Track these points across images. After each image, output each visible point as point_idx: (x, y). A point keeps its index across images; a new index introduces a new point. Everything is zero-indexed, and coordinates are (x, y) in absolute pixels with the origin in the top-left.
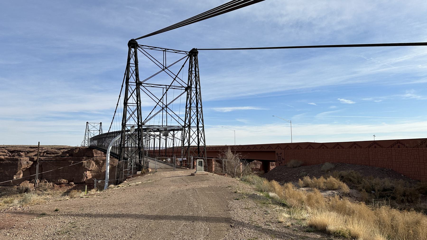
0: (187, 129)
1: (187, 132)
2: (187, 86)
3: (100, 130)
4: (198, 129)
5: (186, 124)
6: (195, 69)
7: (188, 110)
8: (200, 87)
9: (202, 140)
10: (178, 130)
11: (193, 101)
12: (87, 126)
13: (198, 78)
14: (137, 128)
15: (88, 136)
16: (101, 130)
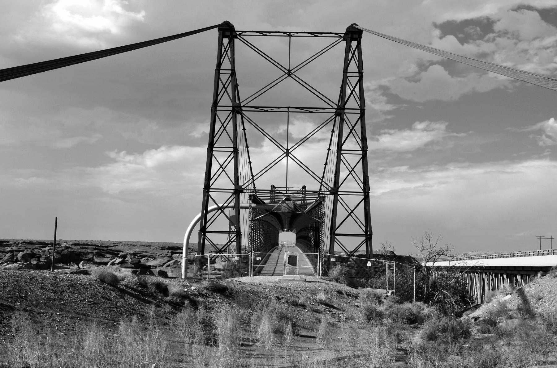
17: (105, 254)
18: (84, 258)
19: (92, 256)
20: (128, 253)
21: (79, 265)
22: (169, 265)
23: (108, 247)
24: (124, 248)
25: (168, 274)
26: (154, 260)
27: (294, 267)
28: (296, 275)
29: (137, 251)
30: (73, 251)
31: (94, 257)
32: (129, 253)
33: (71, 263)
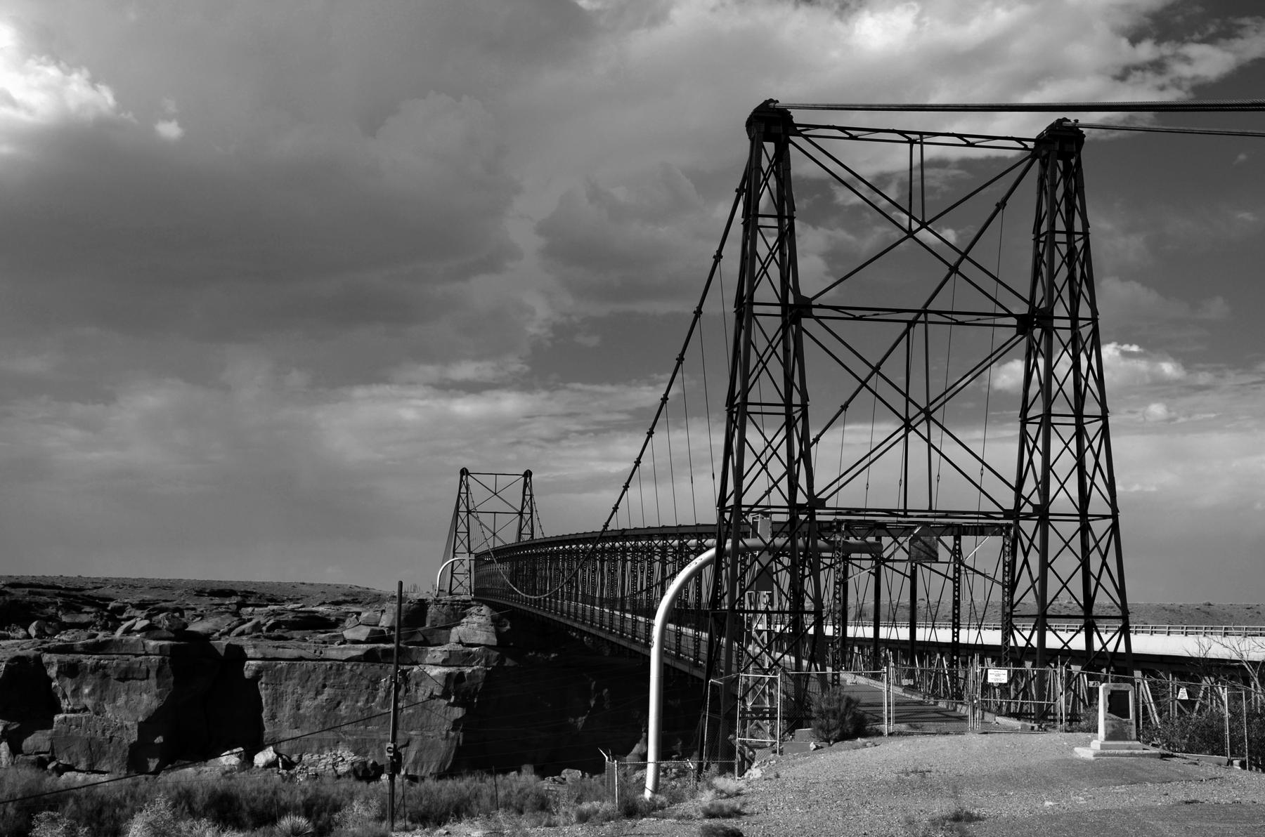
0: (1028, 526)
1: (1035, 446)
2: (1023, 309)
3: (523, 508)
4: (1085, 529)
5: (1023, 501)
6: (1069, 223)
7: (1032, 429)
8: (1095, 312)
9: (1098, 479)
10: (980, 531)
11: (1061, 388)
12: (464, 490)
13: (1082, 268)
14: (784, 518)
15: (466, 542)
16: (527, 510)
17: (82, 606)
18: (38, 614)
19: (54, 611)
20: (127, 603)
21: (29, 630)
22: (244, 631)
23: (81, 589)
24: (117, 592)
25: (246, 651)
26: (201, 619)
27: (1125, 720)
28: (1131, 740)
29: (146, 599)
30: (16, 601)
31: (60, 613)
32: (131, 604)
33: (10, 626)
